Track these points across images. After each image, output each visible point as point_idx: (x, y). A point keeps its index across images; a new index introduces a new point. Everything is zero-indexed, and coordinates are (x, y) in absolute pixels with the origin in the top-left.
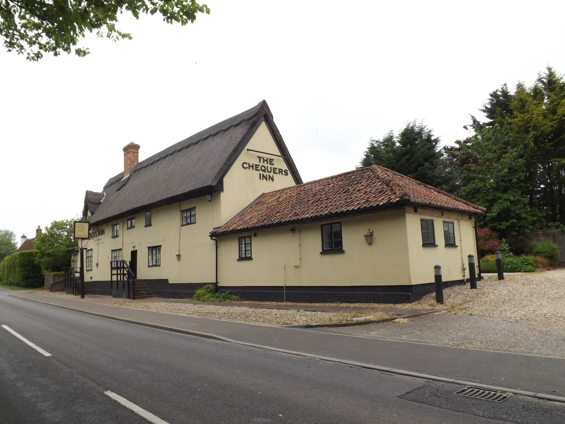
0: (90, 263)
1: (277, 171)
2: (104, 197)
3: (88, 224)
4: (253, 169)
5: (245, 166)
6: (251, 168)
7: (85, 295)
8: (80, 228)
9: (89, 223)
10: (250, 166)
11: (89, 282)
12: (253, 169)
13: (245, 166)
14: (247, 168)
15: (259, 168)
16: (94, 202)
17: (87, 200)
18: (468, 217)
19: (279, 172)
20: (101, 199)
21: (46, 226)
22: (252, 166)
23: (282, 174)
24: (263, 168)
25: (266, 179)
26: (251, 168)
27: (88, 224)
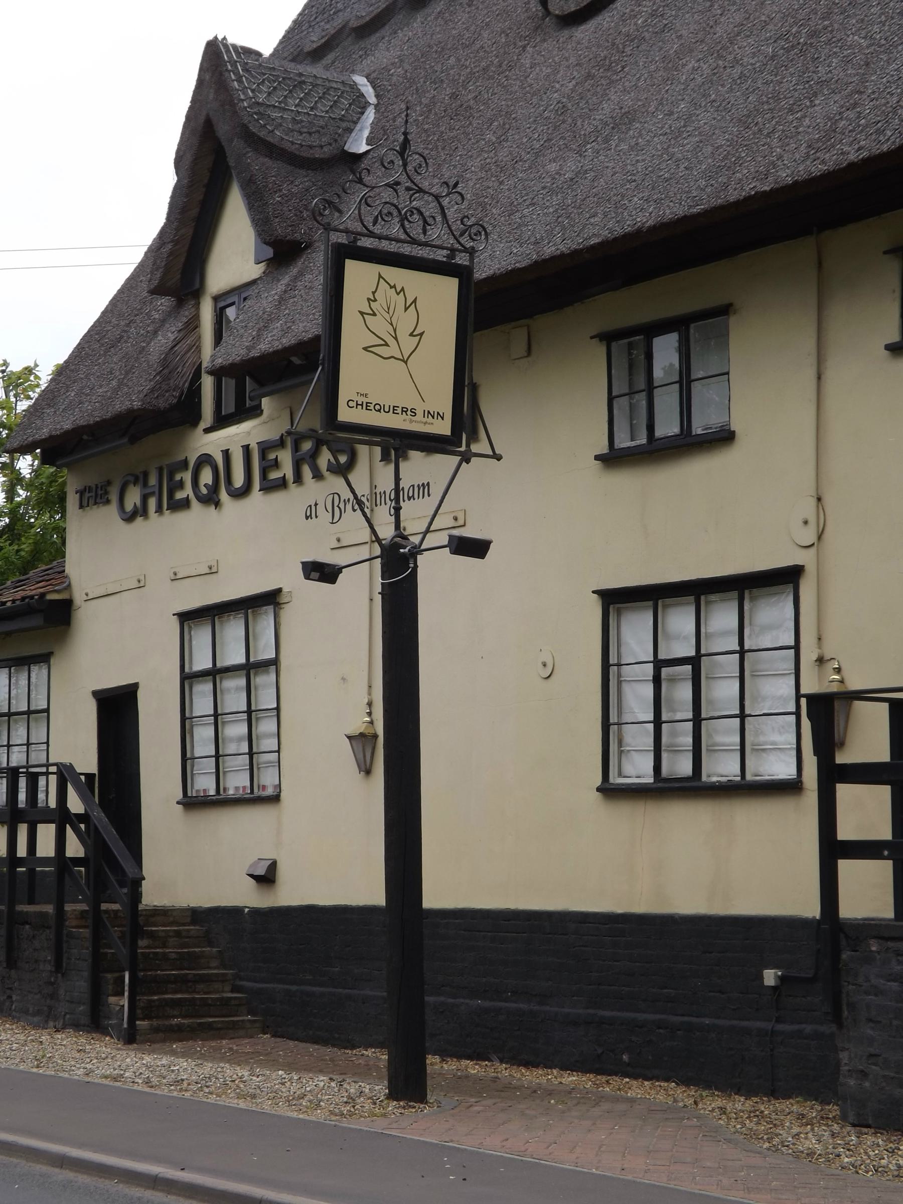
0: (236, 730)
1: (399, 410)
2: (370, 115)
3: (449, 287)
4: (362, 409)
5: (351, 404)
6: (360, 407)
7: (213, 377)
8: (379, 324)
9: (462, 274)
10: (357, 405)
11: (233, 913)
12: (362, 409)
13: (351, 404)
14: (353, 407)
15: (372, 407)
16: (294, 141)
17: (223, 129)
18: (275, 467)
19: (402, 411)
20: (349, 125)
21: (803, 524)
22: (362, 405)
23: (407, 415)
24: (377, 407)
25: (438, 413)
26: (360, 407)
27: (449, 287)
